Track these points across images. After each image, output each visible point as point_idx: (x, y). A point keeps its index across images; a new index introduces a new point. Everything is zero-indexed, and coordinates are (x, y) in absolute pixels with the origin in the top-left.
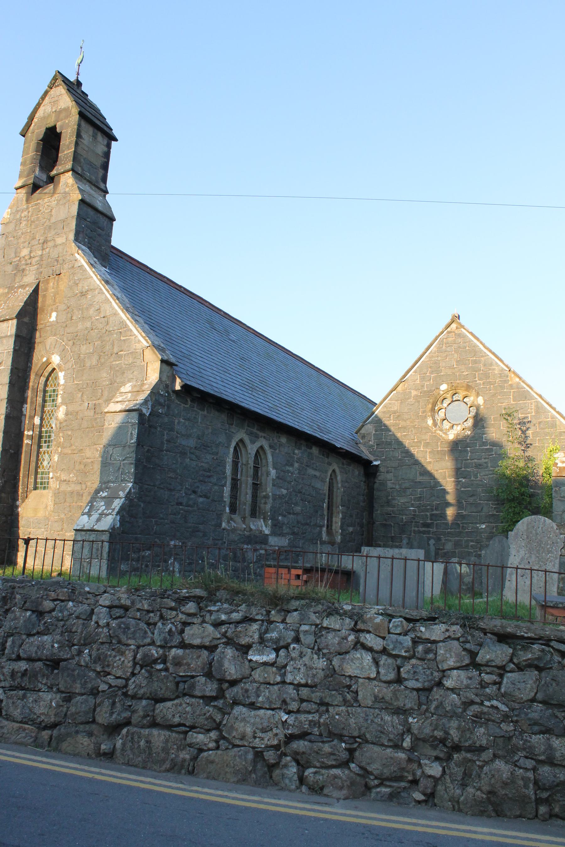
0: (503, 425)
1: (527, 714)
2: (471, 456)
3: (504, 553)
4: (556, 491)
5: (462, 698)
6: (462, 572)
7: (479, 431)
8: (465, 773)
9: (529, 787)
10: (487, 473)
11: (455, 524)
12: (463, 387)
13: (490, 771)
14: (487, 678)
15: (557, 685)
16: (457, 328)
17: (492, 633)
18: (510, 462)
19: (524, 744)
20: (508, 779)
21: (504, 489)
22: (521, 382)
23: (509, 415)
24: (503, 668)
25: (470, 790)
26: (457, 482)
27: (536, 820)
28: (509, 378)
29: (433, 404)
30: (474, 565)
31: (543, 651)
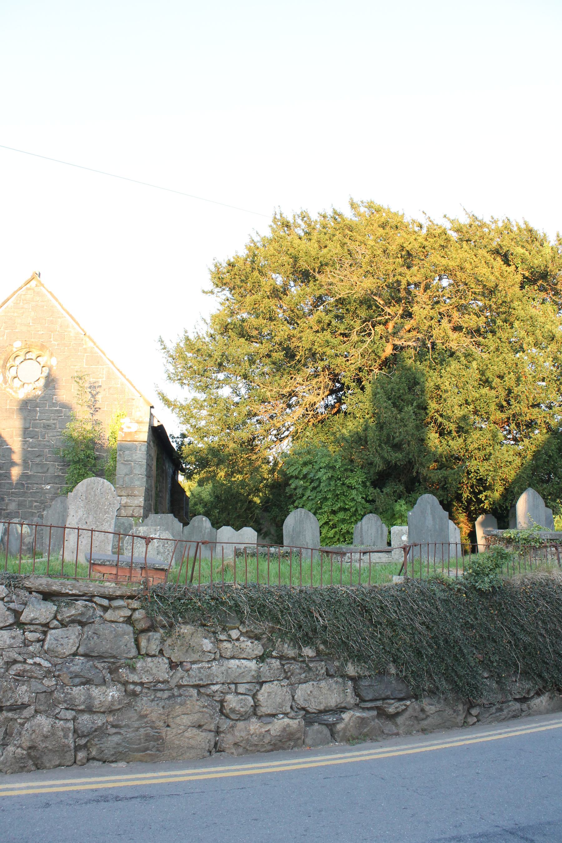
0: (74, 388)
1: (68, 668)
2: (40, 416)
3: (64, 514)
4: (120, 455)
5: (5, 658)
6: (23, 532)
7: (50, 392)
8: (6, 733)
9: (68, 737)
10: (55, 434)
11: (20, 484)
12: (37, 346)
13: (31, 727)
14: (30, 636)
15: (98, 638)
16: (36, 286)
17: (37, 592)
18: (78, 424)
19: (65, 697)
20: (49, 732)
21: (70, 451)
22: (95, 347)
23: (80, 379)
24: (46, 625)
25: (11, 748)
26: (24, 441)
27: (75, 766)
28: (84, 342)
29: (4, 361)
30: (36, 526)
31: (86, 606)
